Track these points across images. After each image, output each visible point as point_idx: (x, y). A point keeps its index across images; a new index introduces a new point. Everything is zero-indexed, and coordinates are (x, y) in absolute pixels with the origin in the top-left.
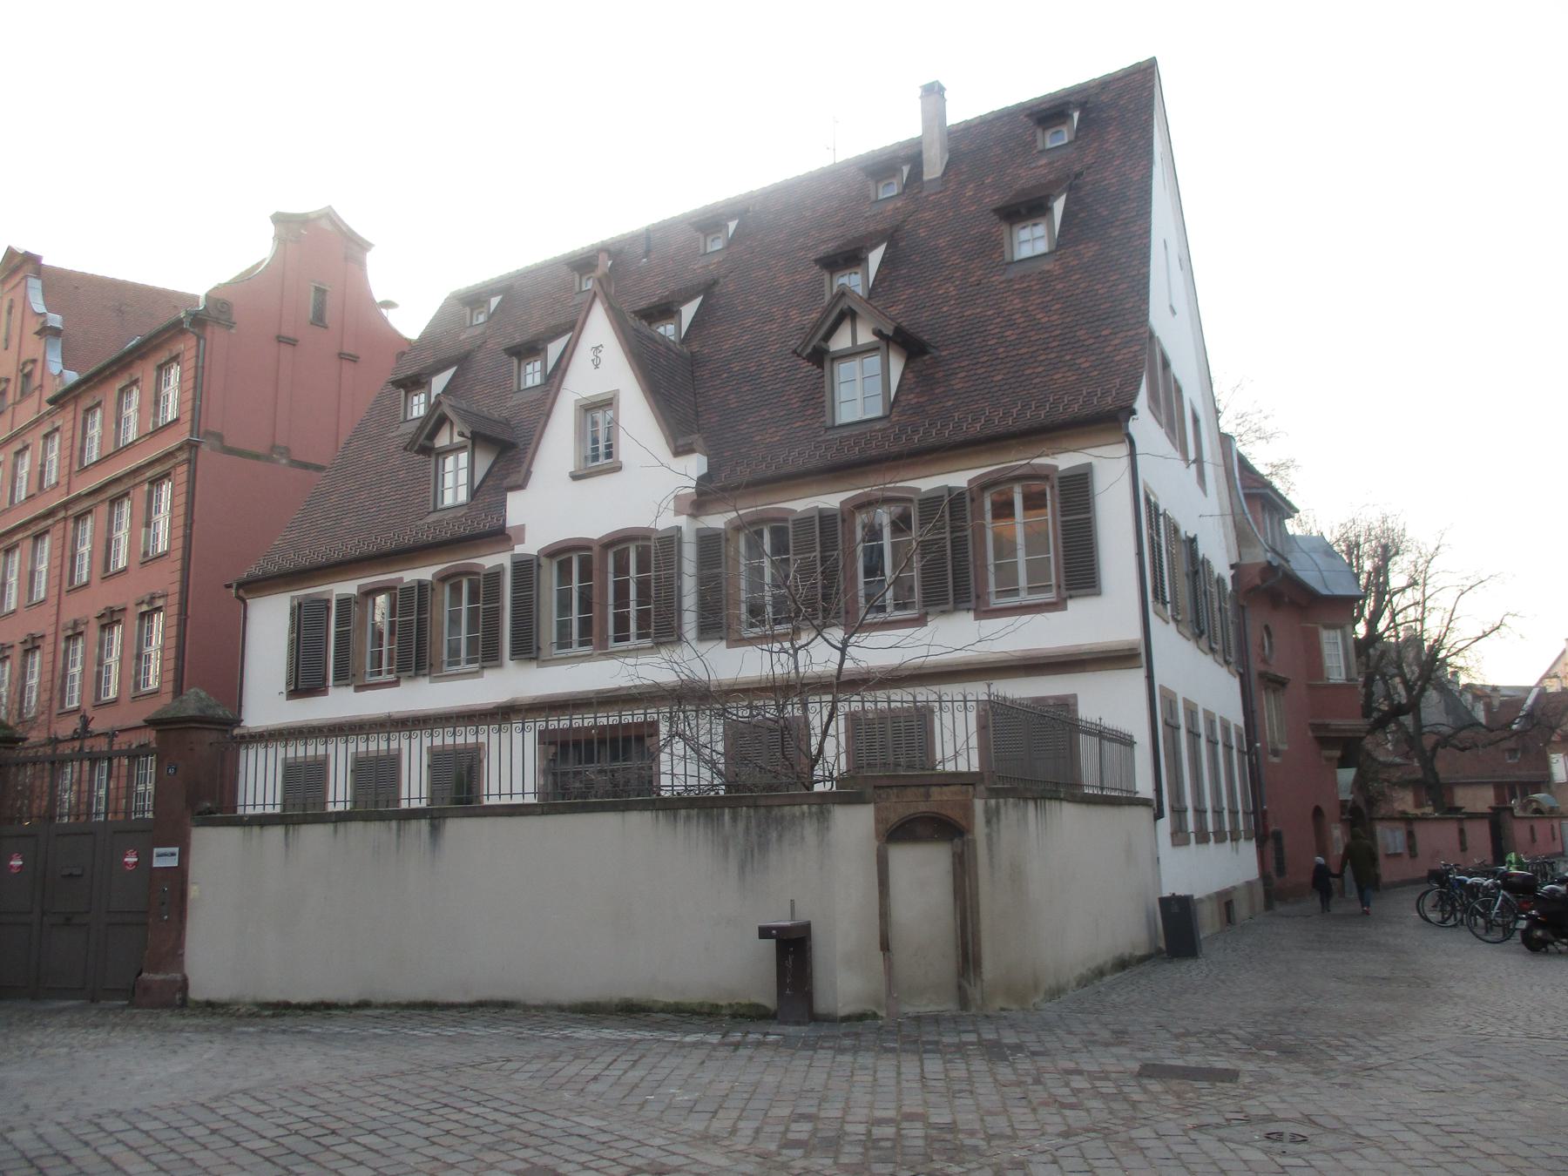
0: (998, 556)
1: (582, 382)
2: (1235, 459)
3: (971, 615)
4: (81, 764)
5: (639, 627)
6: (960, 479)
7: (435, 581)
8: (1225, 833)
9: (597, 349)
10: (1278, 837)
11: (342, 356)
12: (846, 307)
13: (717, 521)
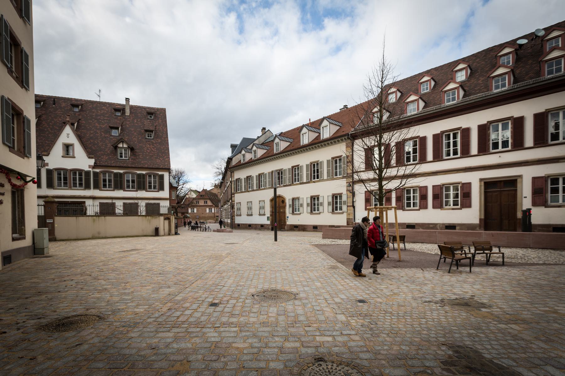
0: (61, 177)
3: (122, 191)
4: (373, 180)
5: (109, 186)
6: (144, 172)
13: (98, 170)
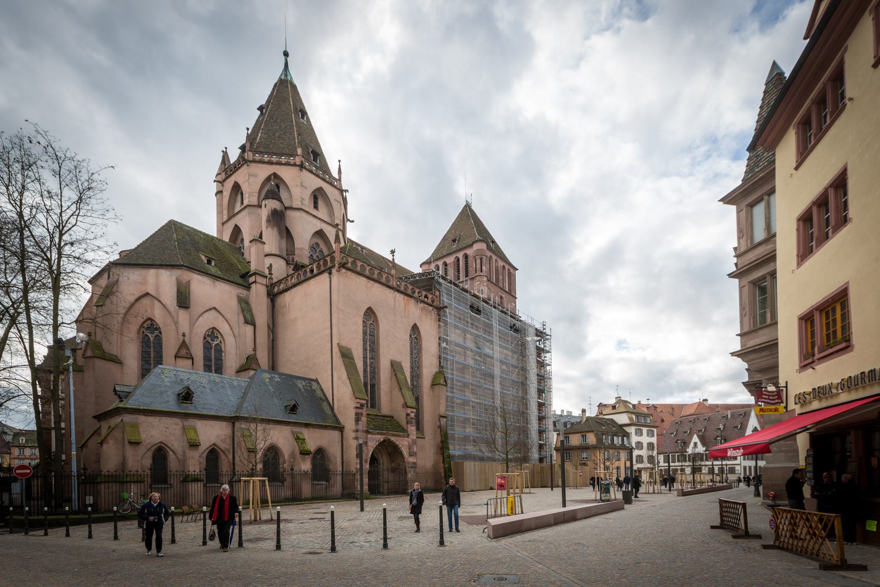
13: (707, 452)
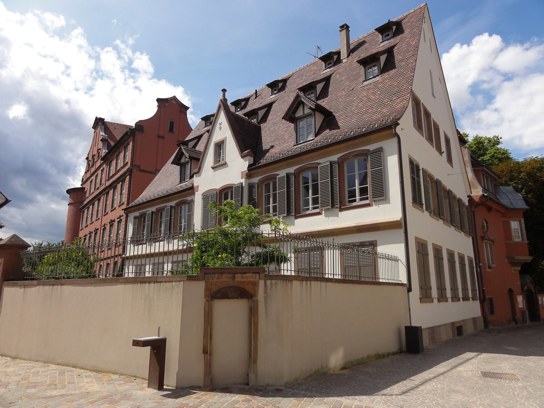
1: (217, 137)
2: (424, 136)
7: (175, 206)
8: (469, 298)
9: (220, 124)
10: (491, 300)
11: (159, 137)
12: (299, 100)
